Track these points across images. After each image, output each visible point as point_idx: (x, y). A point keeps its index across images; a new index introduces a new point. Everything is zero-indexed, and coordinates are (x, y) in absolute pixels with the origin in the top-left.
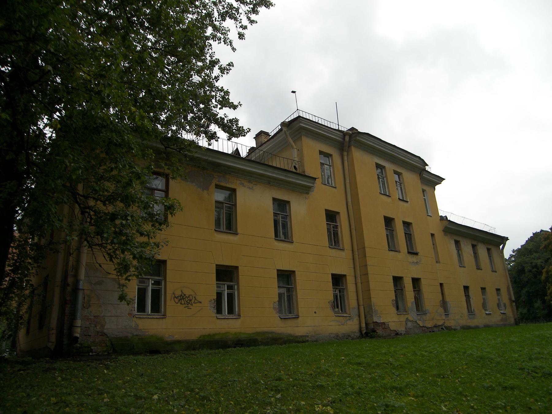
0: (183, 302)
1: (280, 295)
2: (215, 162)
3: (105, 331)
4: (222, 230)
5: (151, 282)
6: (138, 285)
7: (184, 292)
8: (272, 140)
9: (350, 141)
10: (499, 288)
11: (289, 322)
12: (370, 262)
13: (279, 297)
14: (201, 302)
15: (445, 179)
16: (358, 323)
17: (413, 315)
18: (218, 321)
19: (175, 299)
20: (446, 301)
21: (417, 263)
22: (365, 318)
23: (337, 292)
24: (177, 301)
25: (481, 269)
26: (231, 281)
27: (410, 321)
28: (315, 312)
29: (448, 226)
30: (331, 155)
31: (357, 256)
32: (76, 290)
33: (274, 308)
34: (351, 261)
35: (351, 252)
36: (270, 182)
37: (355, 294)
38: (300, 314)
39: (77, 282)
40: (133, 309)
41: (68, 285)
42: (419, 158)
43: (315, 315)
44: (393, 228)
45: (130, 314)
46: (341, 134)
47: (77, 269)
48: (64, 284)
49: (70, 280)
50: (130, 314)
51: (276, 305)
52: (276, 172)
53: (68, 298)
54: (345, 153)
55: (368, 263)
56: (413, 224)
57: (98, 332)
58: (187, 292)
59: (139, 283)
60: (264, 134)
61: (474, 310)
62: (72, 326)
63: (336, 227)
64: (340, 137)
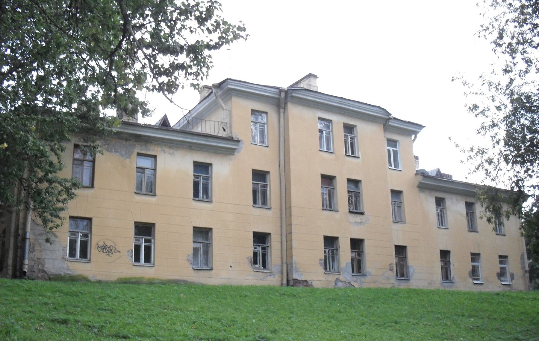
0: (105, 251)
1: (196, 251)
2: (136, 134)
3: (45, 269)
4: (143, 192)
5: (80, 234)
6: (70, 237)
7: (106, 243)
8: (208, 99)
9: (286, 97)
10: (504, 254)
11: (202, 273)
12: (294, 221)
13: (361, 267)
14: (120, 252)
15: (425, 127)
16: (280, 279)
17: (347, 275)
18: (134, 267)
19: (99, 248)
20: (408, 266)
21: (361, 223)
22: (287, 275)
23: (259, 249)
24: (100, 249)
25: (478, 232)
26: (150, 235)
27: (342, 282)
28: (231, 266)
29: (422, 181)
30: (266, 113)
31: (285, 215)
32: (24, 239)
33: (188, 260)
34: (279, 220)
35: (279, 211)
36: (191, 147)
37: (279, 252)
38: (214, 267)
39: (25, 233)
40: (65, 254)
41: (19, 235)
42: (379, 107)
43: (230, 268)
44: (333, 186)
45: (63, 258)
46: (277, 90)
47: (25, 224)
48: (17, 235)
49: (20, 232)
50: (63, 258)
51: (191, 258)
52: (196, 137)
53: (19, 245)
54: (282, 110)
55: (292, 223)
56: (363, 182)
57: (40, 270)
58: (108, 243)
59: (71, 235)
60: (207, 88)
61: (453, 277)
62: (22, 264)
63: (265, 186)
64: (276, 94)
